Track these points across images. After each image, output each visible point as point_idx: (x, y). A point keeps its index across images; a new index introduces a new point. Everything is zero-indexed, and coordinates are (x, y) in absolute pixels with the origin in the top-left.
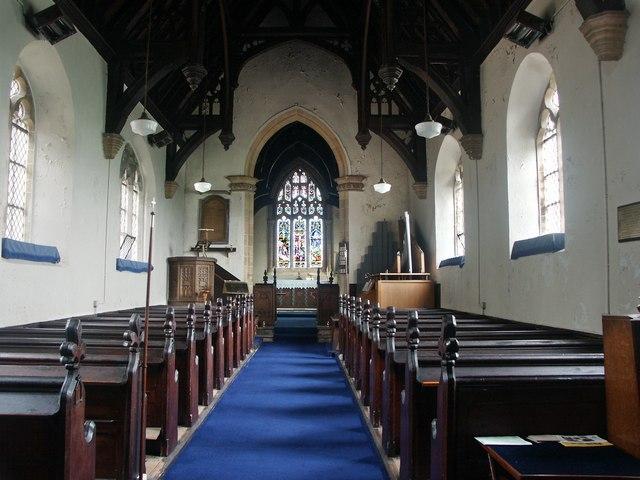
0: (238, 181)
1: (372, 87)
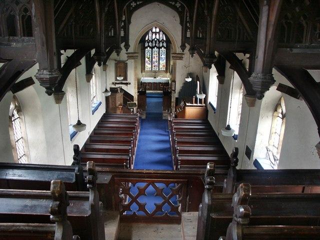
0: (131, 55)
1: (188, 25)
